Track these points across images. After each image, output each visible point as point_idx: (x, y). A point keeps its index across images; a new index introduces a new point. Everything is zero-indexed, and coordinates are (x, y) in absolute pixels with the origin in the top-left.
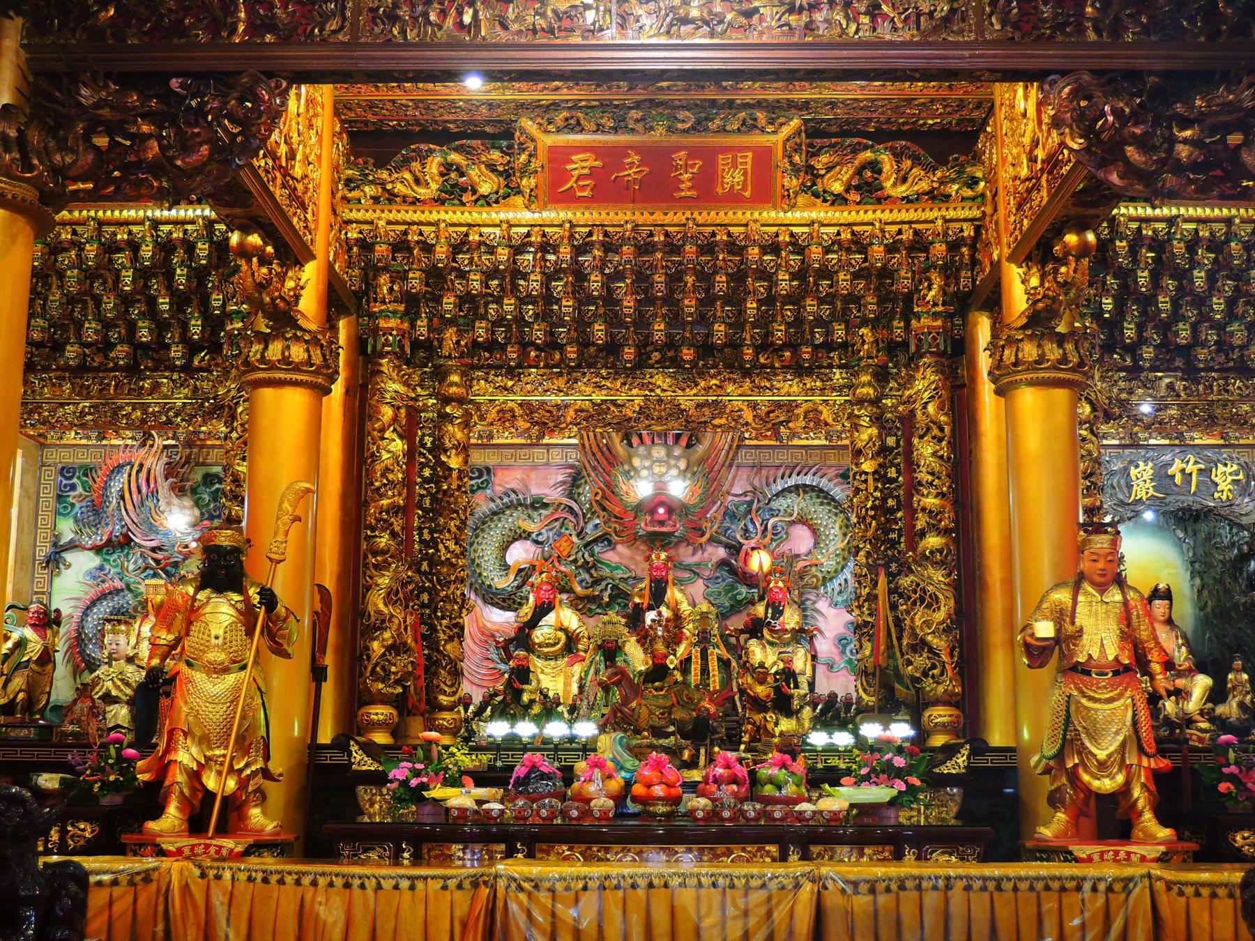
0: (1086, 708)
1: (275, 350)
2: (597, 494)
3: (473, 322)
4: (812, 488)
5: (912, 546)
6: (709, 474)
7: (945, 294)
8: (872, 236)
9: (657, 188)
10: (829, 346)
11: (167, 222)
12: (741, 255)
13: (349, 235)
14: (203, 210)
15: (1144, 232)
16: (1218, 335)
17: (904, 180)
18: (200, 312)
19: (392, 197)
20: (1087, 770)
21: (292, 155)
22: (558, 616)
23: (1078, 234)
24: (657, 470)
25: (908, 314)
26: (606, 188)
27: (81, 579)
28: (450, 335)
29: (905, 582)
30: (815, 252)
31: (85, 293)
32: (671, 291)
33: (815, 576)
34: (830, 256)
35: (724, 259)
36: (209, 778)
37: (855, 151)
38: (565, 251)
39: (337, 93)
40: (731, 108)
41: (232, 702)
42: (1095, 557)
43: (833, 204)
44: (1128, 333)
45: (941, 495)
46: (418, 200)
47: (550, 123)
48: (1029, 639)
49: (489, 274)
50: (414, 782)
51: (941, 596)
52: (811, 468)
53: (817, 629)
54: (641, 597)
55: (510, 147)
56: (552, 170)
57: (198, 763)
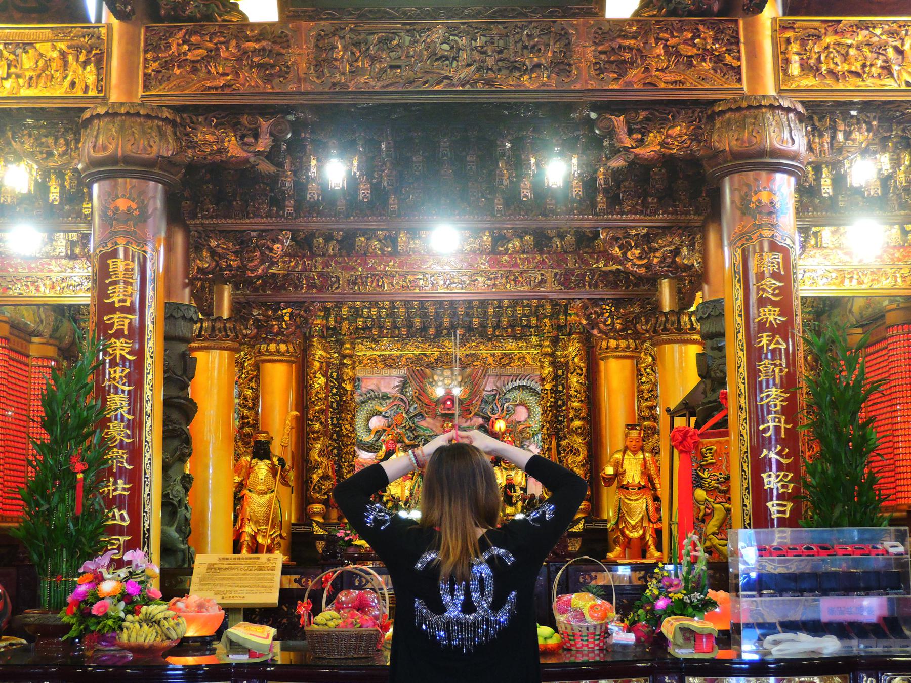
4: (527, 387)
6: (472, 383)
28: (345, 324)
29: (564, 443)
50: (346, 539)
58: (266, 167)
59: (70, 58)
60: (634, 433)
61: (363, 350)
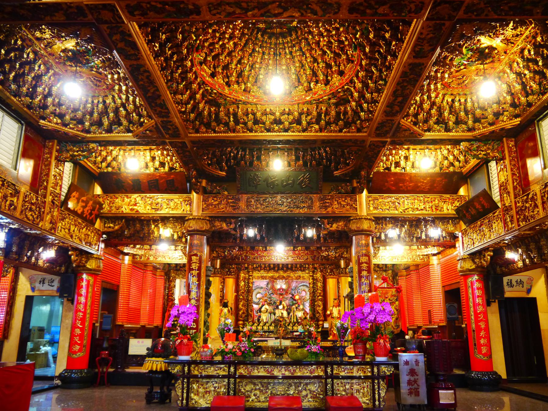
29: (316, 303)
58: (233, 232)
59: (183, 203)
60: (336, 301)
61: (256, 274)
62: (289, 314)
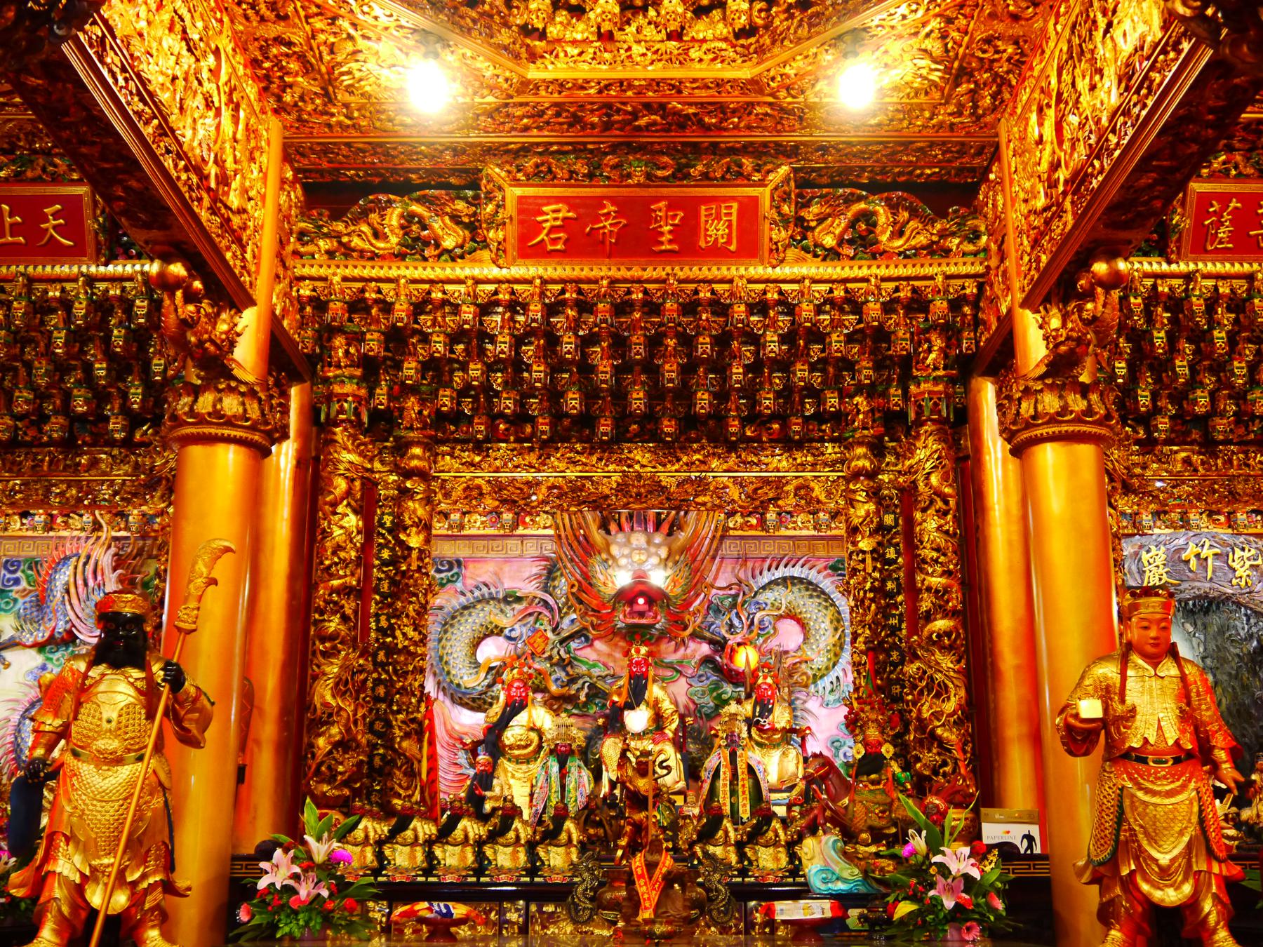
0: (1144, 802)
1: (205, 402)
2: (573, 586)
3: (437, 390)
4: (801, 580)
5: (914, 630)
6: (692, 563)
7: (946, 357)
8: (867, 293)
9: (636, 241)
10: (820, 417)
11: (104, 279)
12: (726, 315)
13: (302, 292)
14: (143, 265)
15: (1160, 289)
16: (1237, 405)
17: (900, 234)
18: (141, 380)
19: (348, 251)
20: (1147, 880)
21: (224, 180)
22: (530, 716)
23: (1108, 262)
24: (636, 558)
25: (906, 379)
26: (580, 241)
27: (21, 680)
30: (806, 310)
31: (15, 358)
32: (651, 355)
33: (805, 674)
34: (822, 317)
35: (707, 320)
36: (94, 893)
37: (849, 201)
38: (536, 310)
39: (287, 134)
40: (714, 154)
41: (126, 799)
42: (1146, 624)
43: (824, 260)
44: (1142, 401)
45: (947, 573)
46: (376, 255)
47: (519, 171)
48: (1072, 721)
49: (455, 337)
51: (950, 685)
52: (799, 559)
53: (809, 728)
54: (619, 695)
55: (476, 197)
56: (521, 222)
57: (82, 875)
62: (692, 771)
